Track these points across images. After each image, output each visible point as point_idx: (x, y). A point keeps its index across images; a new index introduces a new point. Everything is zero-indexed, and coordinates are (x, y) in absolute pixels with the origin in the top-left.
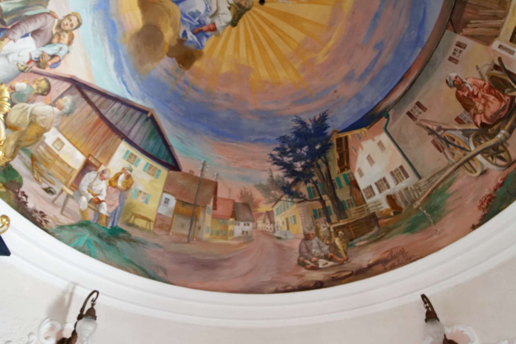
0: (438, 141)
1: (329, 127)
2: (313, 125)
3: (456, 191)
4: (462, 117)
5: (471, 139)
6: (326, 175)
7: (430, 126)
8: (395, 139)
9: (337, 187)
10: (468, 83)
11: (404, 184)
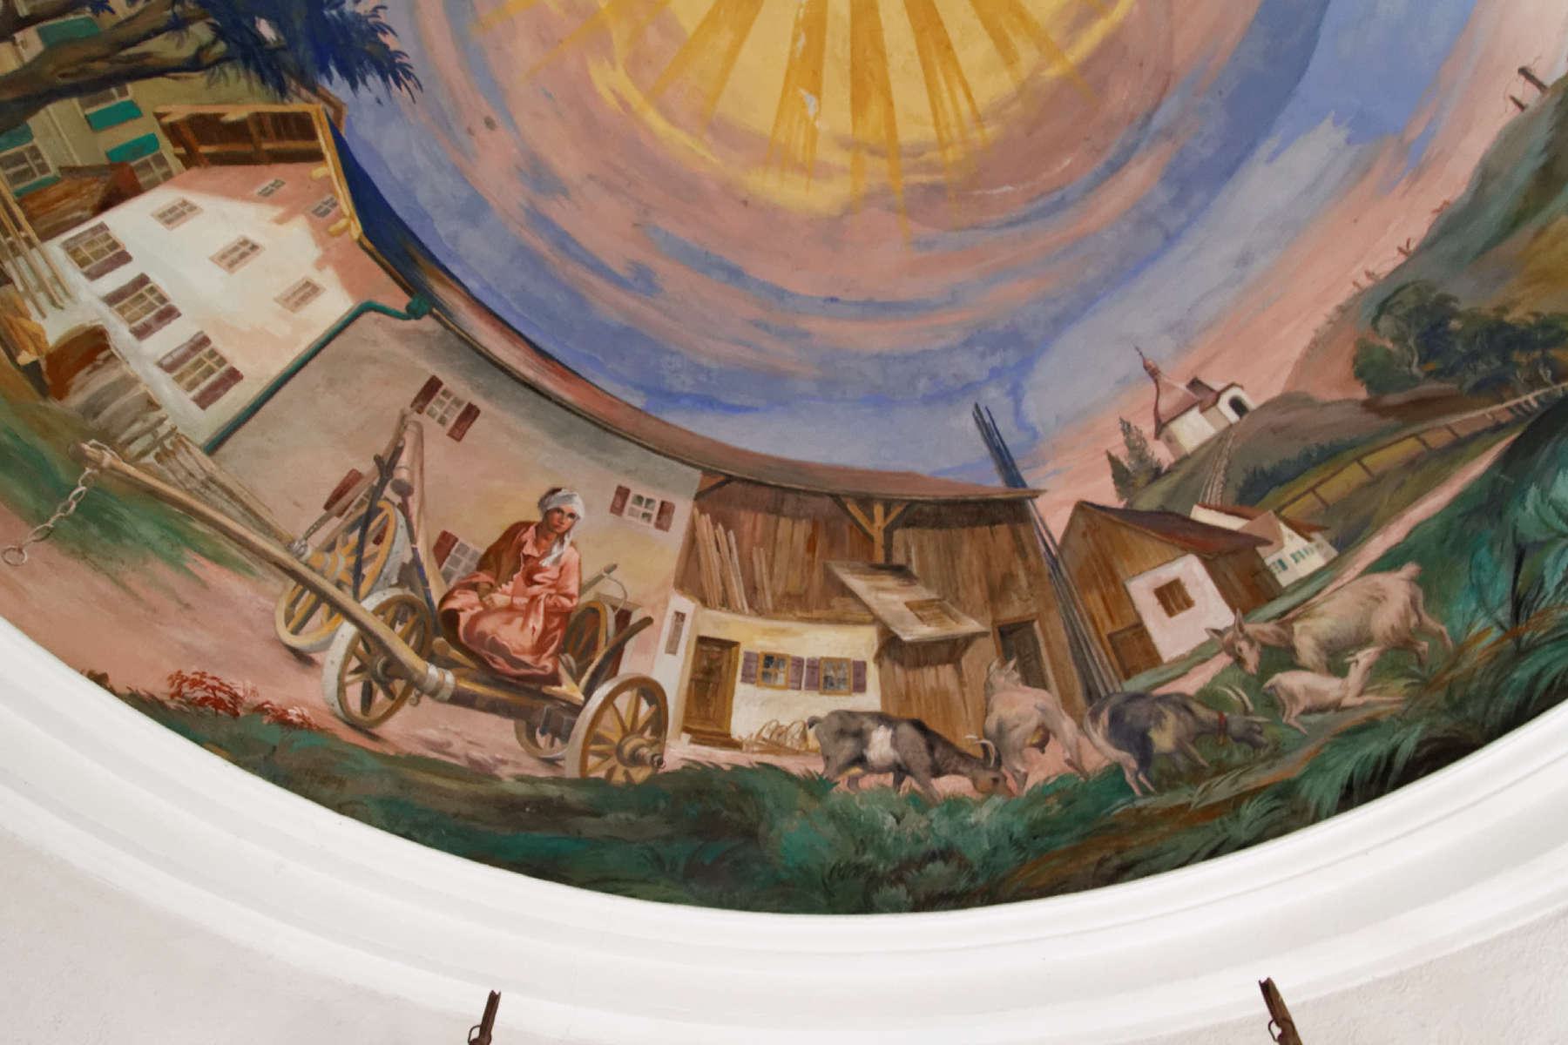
0: (360, 492)
1: (354, 86)
2: (357, 16)
3: (204, 585)
4: (457, 551)
5: (397, 592)
6: (147, 55)
7: (404, 459)
8: (334, 344)
9: (95, 103)
10: (563, 552)
11: (174, 398)
